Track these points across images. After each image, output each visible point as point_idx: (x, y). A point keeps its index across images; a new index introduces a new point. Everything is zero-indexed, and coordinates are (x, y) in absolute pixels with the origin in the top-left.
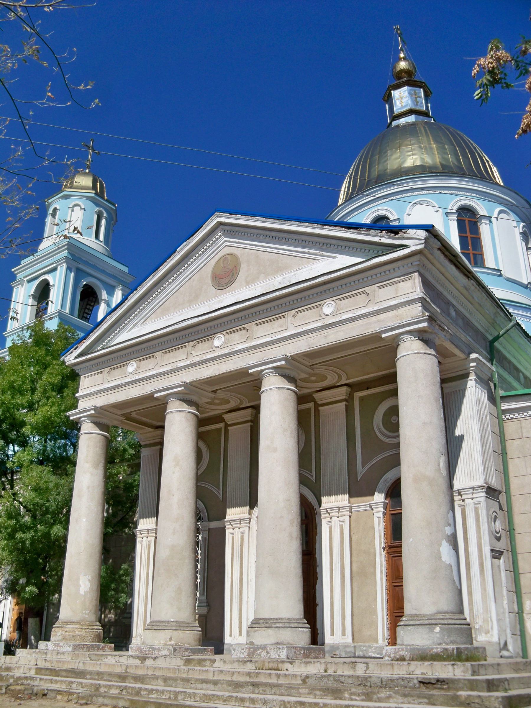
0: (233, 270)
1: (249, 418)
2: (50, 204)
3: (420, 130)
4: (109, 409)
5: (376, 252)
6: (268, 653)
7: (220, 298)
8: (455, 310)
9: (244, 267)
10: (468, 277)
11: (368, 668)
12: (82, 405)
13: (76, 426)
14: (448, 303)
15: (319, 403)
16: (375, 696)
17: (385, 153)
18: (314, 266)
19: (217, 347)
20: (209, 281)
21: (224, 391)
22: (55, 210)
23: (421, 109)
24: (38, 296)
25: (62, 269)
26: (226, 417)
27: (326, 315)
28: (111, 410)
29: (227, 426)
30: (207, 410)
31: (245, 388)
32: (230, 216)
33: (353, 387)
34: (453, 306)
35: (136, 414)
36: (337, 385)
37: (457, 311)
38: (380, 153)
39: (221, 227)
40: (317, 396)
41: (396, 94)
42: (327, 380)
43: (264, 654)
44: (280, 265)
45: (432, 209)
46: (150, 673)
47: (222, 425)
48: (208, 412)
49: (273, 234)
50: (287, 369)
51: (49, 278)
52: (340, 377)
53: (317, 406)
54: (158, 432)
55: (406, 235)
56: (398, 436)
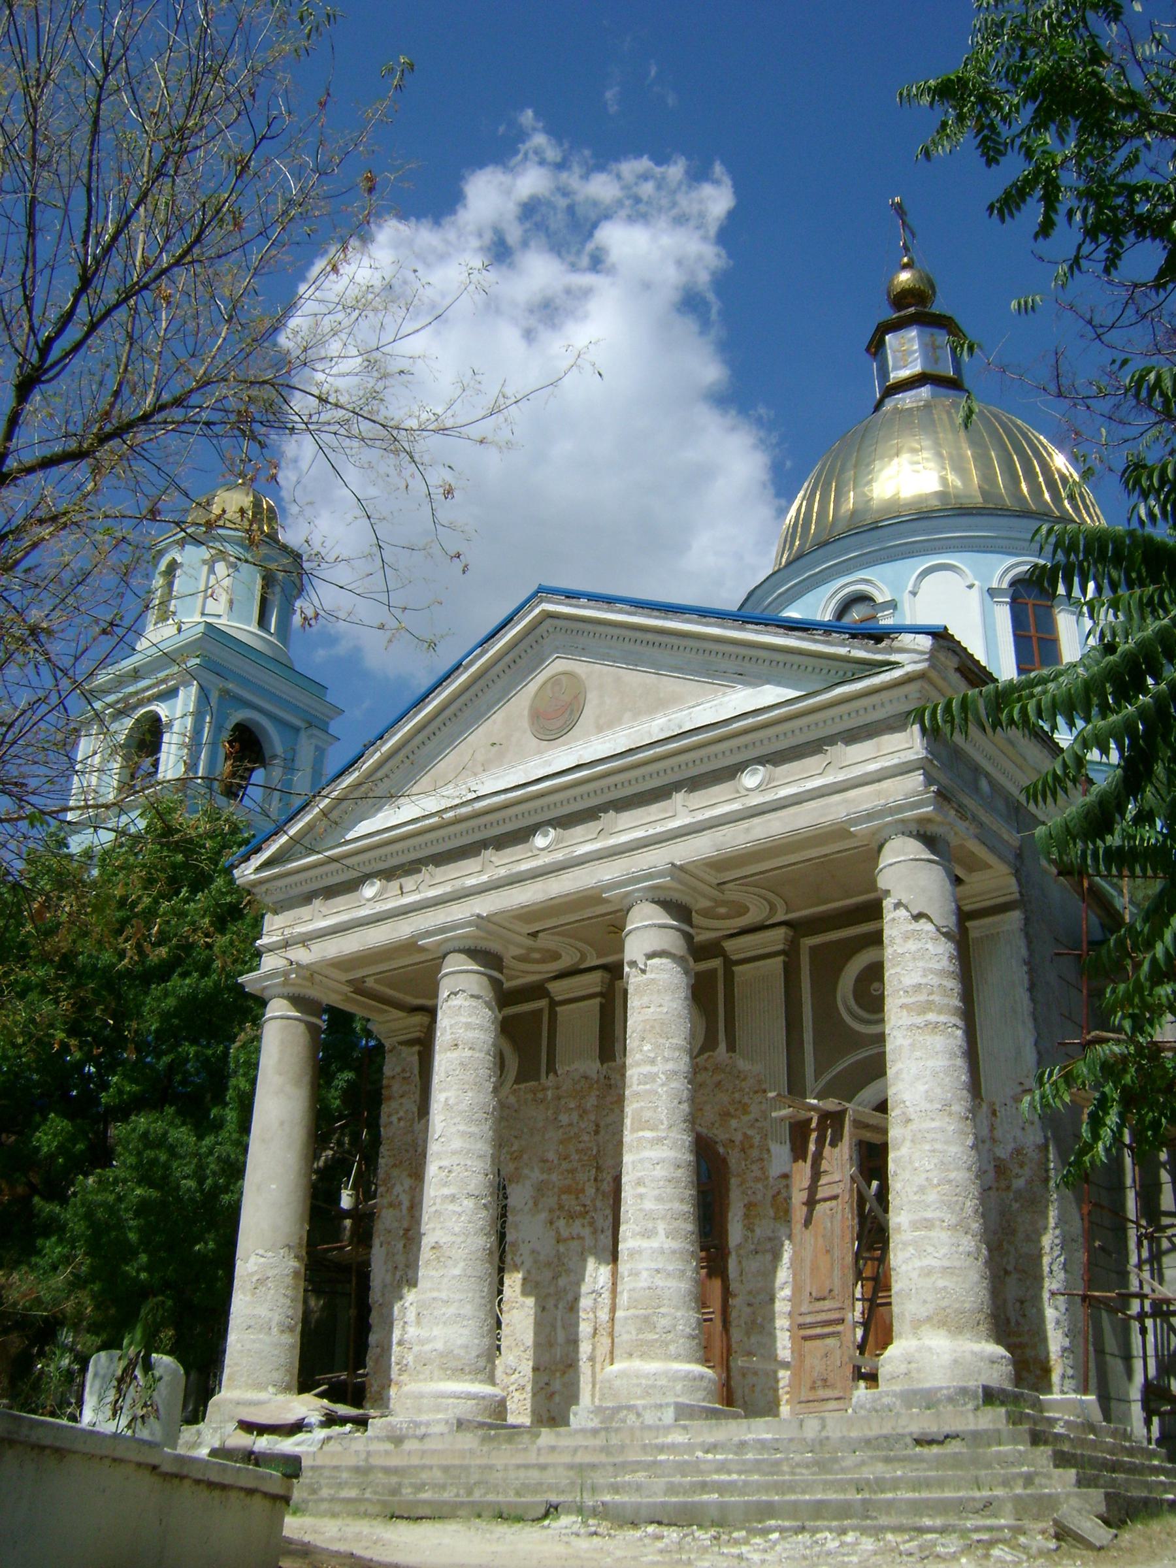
1: (598, 989)
3: (941, 419)
5: (841, 673)
6: (638, 1415)
7: (547, 756)
8: (990, 782)
9: (592, 699)
11: (824, 1427)
12: (270, 963)
14: (977, 770)
15: (734, 957)
16: (836, 1467)
17: (868, 465)
18: (726, 699)
20: (525, 723)
22: (173, 566)
23: (943, 373)
26: (553, 987)
27: (748, 790)
29: (553, 1004)
33: (799, 928)
34: (987, 775)
35: (376, 981)
37: (992, 782)
38: (856, 466)
39: (549, 621)
40: (729, 945)
43: (632, 1418)
45: (961, 583)
46: (415, 1461)
47: (543, 1003)
49: (650, 637)
50: (675, 890)
51: (162, 710)
52: (773, 908)
53: (729, 964)
55: (896, 644)
56: (882, 1021)
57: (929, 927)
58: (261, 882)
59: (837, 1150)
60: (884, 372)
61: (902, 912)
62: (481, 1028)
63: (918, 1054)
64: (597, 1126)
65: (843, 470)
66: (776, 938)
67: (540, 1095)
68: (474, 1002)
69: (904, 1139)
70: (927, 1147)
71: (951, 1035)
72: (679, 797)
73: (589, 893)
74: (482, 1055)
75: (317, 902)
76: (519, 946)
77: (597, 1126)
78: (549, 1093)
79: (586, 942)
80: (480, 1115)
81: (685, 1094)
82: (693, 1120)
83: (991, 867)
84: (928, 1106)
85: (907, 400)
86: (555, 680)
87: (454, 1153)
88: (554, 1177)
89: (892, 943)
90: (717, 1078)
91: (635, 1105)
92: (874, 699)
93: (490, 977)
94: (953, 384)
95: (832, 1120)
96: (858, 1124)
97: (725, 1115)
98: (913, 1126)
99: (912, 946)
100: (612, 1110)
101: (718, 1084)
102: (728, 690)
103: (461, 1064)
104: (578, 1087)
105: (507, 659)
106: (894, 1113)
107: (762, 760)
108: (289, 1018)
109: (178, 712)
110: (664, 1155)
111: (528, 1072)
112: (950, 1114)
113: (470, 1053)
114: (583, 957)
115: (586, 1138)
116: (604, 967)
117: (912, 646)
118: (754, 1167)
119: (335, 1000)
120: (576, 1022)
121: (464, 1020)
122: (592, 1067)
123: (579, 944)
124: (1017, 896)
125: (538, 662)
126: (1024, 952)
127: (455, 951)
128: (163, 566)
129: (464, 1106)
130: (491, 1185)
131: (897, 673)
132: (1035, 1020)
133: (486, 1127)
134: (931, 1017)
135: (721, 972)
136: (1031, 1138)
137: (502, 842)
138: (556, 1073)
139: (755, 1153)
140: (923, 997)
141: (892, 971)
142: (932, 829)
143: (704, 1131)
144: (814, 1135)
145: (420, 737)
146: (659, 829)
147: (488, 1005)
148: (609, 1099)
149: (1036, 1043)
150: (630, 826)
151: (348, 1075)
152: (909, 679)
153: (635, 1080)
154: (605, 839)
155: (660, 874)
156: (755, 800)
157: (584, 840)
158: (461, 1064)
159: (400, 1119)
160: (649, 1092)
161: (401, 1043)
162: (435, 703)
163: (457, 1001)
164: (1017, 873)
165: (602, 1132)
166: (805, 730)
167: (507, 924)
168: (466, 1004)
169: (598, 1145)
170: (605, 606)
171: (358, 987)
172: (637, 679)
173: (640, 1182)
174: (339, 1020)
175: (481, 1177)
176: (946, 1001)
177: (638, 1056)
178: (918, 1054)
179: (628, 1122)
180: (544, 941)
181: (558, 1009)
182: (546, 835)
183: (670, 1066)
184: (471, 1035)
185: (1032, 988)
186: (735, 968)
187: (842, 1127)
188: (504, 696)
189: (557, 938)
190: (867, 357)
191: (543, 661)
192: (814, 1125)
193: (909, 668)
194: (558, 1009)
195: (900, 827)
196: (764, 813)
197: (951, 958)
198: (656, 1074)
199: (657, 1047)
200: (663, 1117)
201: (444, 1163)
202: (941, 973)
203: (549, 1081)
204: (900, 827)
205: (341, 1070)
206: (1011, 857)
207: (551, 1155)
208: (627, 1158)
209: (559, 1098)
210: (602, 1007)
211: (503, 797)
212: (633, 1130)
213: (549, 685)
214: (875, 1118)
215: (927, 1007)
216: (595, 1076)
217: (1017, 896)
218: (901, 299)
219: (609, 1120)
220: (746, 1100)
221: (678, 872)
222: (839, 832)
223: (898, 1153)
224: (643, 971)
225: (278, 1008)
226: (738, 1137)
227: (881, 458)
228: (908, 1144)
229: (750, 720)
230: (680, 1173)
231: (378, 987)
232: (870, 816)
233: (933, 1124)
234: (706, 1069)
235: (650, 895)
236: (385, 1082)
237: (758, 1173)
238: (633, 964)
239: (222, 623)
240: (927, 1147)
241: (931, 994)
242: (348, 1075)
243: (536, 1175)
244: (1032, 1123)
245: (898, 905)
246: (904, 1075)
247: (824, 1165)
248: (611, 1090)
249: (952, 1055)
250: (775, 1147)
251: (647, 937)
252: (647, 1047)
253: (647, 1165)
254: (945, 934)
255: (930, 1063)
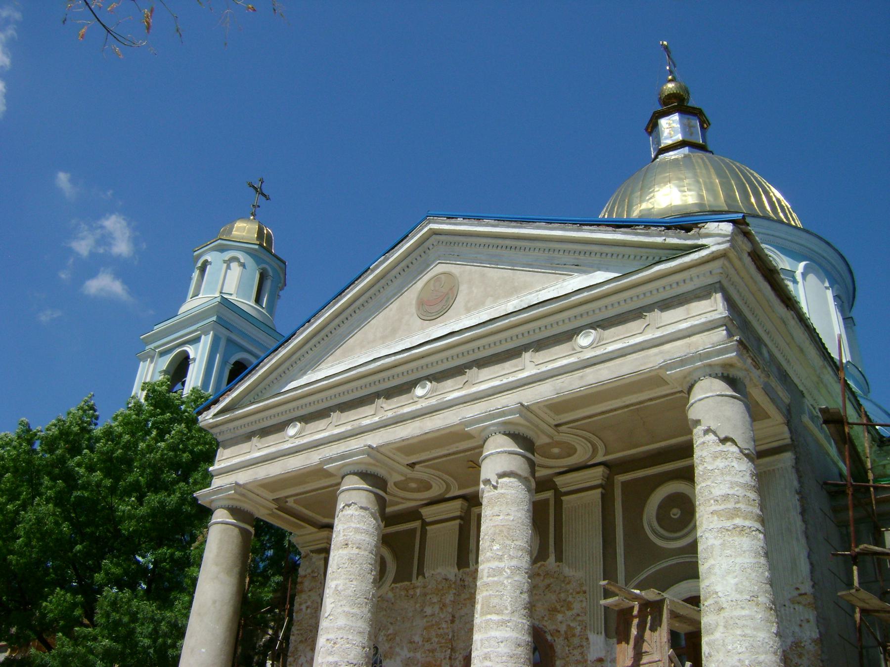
0: (447, 294)
1: (458, 514)
2: (200, 256)
3: (697, 162)
4: (256, 491)
10: (787, 306)
12: (217, 482)
13: (205, 513)
14: (759, 340)
15: (563, 490)
18: (565, 283)
19: (421, 397)
20: (413, 310)
21: (427, 467)
22: (206, 263)
23: (697, 142)
24: (172, 372)
25: (206, 341)
26: (425, 511)
27: (582, 347)
28: (259, 492)
29: (425, 524)
30: (397, 499)
31: (457, 458)
32: (448, 221)
34: (766, 345)
35: (296, 502)
36: (590, 463)
37: (769, 352)
38: (641, 189)
39: (434, 237)
40: (559, 480)
41: (664, 122)
42: (575, 456)
44: (516, 284)
47: (417, 524)
48: (397, 503)
49: (508, 242)
51: (190, 350)
54: (324, 533)
55: (703, 231)
57: (734, 449)
58: (216, 425)
59: (657, 634)
60: (658, 141)
61: (711, 437)
62: (367, 532)
63: (728, 552)
64: (453, 617)
65: (632, 193)
66: (596, 475)
67: (411, 592)
68: (363, 513)
69: (717, 625)
70: (739, 632)
71: (755, 537)
72: (527, 356)
73: (452, 430)
74: (367, 553)
75: (255, 440)
76: (402, 474)
77: (453, 617)
78: (418, 591)
79: (452, 477)
80: (362, 600)
81: (526, 587)
82: (531, 608)
83: (769, 417)
84: (738, 596)
85: (672, 155)
86: (436, 278)
87: (339, 629)
88: (418, 655)
89: (703, 461)
90: (547, 581)
91: (485, 593)
92: (685, 275)
93: (376, 494)
94: (702, 148)
95: (652, 609)
96: (674, 615)
97: (553, 611)
98: (725, 614)
99: (720, 463)
100: (465, 605)
101: (548, 586)
102: (567, 277)
103: (350, 559)
104: (440, 587)
105: (403, 264)
106: (707, 603)
107: (594, 326)
108: (227, 523)
109: (199, 353)
110: (507, 635)
111: (403, 575)
112: (757, 604)
113: (357, 551)
114: (448, 489)
115: (444, 626)
116: (463, 497)
117: (716, 232)
118: (575, 652)
119: (262, 514)
120: (441, 538)
121: (353, 525)
122: (451, 571)
123: (446, 477)
124: (788, 441)
125: (426, 266)
126: (796, 483)
127: (350, 474)
128: (199, 264)
129: (349, 592)
130: (367, 657)
131: (704, 253)
132: (807, 538)
133: (366, 610)
134: (738, 521)
135: (552, 502)
136: (808, 633)
137: (390, 393)
138: (424, 576)
139: (576, 641)
140: (730, 505)
141: (703, 484)
142: (733, 373)
143: (537, 623)
144: (636, 621)
145: (337, 321)
146: (511, 379)
147: (373, 515)
148: (463, 596)
149: (809, 557)
150: (488, 378)
151: (278, 578)
152: (713, 258)
153: (485, 573)
154: (470, 387)
155: (511, 412)
156: (589, 354)
157: (452, 390)
158: (350, 559)
159: (307, 607)
160: (496, 583)
161: (312, 551)
162: (349, 296)
163: (349, 511)
164: (788, 423)
165: (457, 621)
166: (629, 301)
167: (391, 455)
168: (357, 513)
169: (453, 632)
170: (476, 222)
171: (281, 505)
172: (495, 274)
173: (486, 657)
174: (262, 528)
175: (359, 649)
176: (750, 509)
177: (489, 554)
178: (728, 552)
179: (478, 607)
180: (420, 473)
181: (428, 528)
182: (424, 387)
183: (514, 563)
184: (359, 537)
185: (803, 513)
186: (563, 498)
187: (661, 615)
188: (399, 292)
189: (428, 470)
190: (646, 135)
191: (430, 265)
192: (635, 612)
193: (714, 249)
194: (428, 528)
195: (708, 370)
196: (595, 364)
197: (752, 475)
198: (503, 569)
199: (504, 546)
200: (507, 604)
201: (331, 636)
202: (745, 486)
203: (418, 582)
204: (708, 370)
205: (274, 575)
206: (784, 410)
207: (417, 639)
208: (477, 637)
209: (425, 595)
210: (461, 527)
211: (393, 358)
212: (483, 614)
213: (432, 282)
214: (686, 610)
215: (733, 514)
216: (453, 578)
217: (788, 441)
218: (672, 96)
219: (462, 612)
220: (570, 599)
221: (525, 411)
222: (654, 379)
223: (712, 637)
224: (495, 487)
225: (220, 516)
226: (563, 628)
227: (659, 184)
228: (721, 629)
229: (586, 294)
230: (520, 650)
231: (295, 506)
232: (683, 362)
233: (744, 613)
234: (539, 575)
235: (502, 429)
236: (299, 580)
237: (579, 657)
238: (487, 482)
239: (232, 298)
240: (739, 632)
241: (738, 502)
242: (278, 578)
243: (405, 653)
244: (808, 621)
245: (707, 431)
246: (716, 570)
247: (646, 647)
248: (464, 591)
249: (757, 554)
250: (592, 637)
251: (499, 459)
252: (496, 547)
253: (493, 643)
254: (746, 455)
255: (739, 560)
